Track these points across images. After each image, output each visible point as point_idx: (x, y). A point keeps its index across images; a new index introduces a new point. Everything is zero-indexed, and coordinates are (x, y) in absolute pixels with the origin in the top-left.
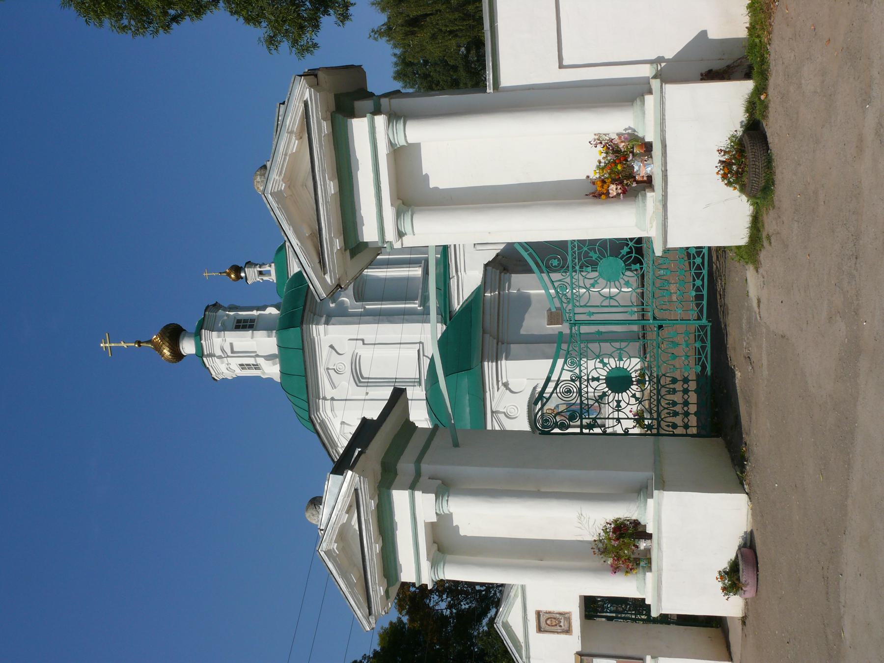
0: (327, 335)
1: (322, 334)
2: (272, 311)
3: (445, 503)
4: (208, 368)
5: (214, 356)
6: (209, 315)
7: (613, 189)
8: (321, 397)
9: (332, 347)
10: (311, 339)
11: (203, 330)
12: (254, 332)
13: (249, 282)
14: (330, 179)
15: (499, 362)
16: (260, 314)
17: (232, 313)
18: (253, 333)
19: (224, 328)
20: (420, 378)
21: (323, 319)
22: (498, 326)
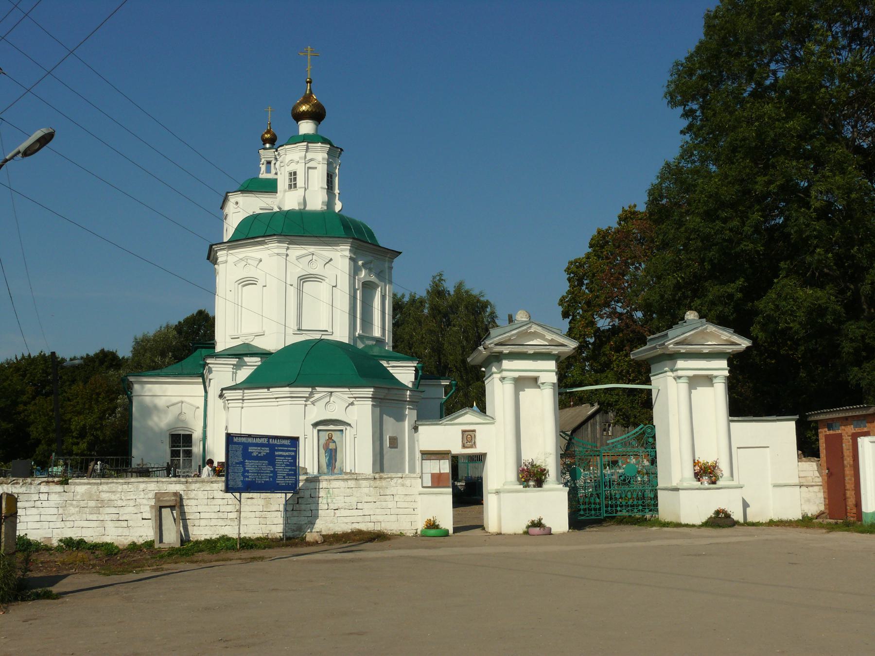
0: (341, 258)
1: (339, 254)
2: (338, 206)
3: (550, 387)
4: (296, 144)
5: (306, 152)
6: (337, 151)
7: (697, 468)
8: (289, 246)
9: (331, 260)
10: (339, 244)
11: (329, 146)
12: (326, 190)
13: (261, 151)
14: (709, 351)
15: (371, 399)
16: (336, 195)
17: (337, 171)
18: (325, 189)
19: (329, 164)
20: (301, 330)
21: (353, 256)
22: (394, 400)
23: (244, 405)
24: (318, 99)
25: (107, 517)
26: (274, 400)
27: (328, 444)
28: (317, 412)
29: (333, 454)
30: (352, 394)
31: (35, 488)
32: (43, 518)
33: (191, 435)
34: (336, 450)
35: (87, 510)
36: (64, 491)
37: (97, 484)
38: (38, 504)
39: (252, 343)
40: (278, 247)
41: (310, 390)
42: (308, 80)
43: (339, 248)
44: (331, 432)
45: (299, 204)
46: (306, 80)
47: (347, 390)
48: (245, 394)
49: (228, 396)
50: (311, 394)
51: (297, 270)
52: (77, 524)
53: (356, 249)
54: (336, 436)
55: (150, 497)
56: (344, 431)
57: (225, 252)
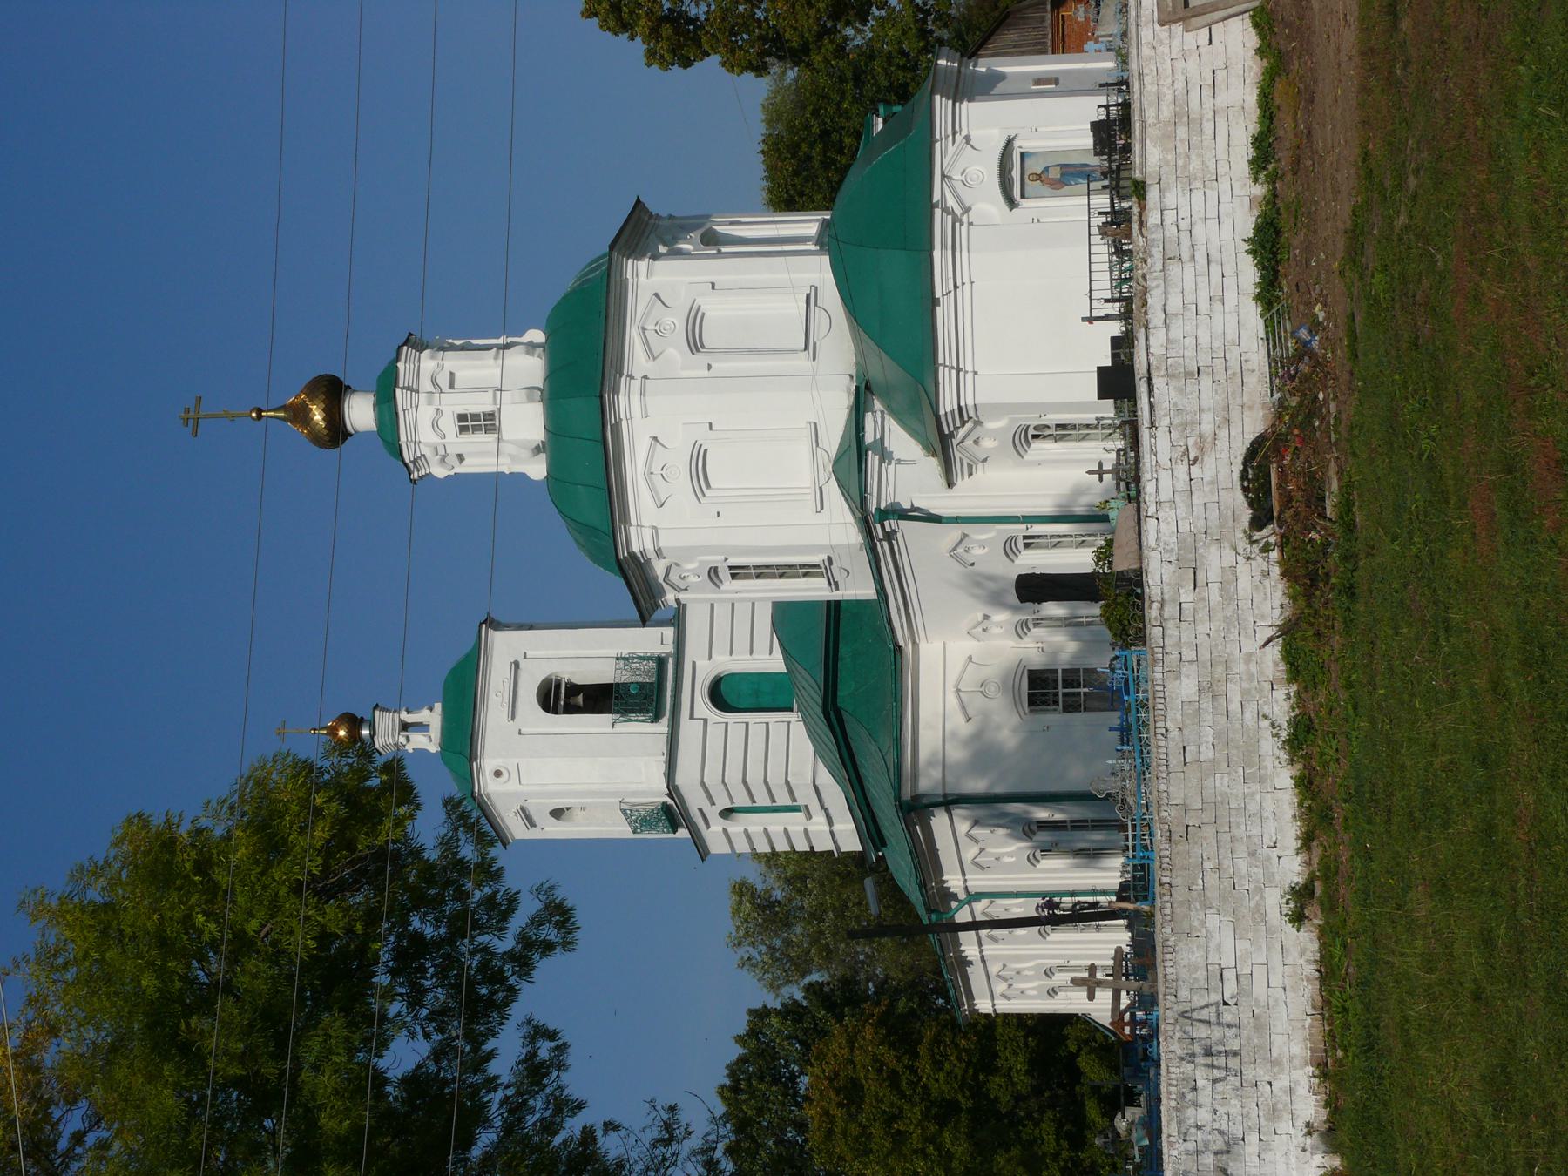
1: (642, 278)
4: (397, 414)
15: (958, 104)
23: (969, 368)
24: (298, 392)
25: (1209, 104)
26: (958, 254)
27: (1047, 432)
28: (987, 203)
29: (1072, 170)
30: (947, 137)
31: (1153, 233)
32: (1212, 213)
33: (1031, 672)
34: (1063, 166)
35: (1194, 140)
36: (1159, 183)
37: (1143, 128)
38: (1184, 225)
39: (833, 451)
40: (628, 394)
41: (938, 212)
42: (254, 415)
43: (631, 281)
44: (1026, 177)
45: (530, 400)
46: (253, 418)
47: (937, 145)
48: (947, 364)
49: (951, 402)
50: (946, 210)
51: (675, 350)
52: (1222, 155)
53: (633, 252)
54: (1034, 167)
55: (1167, 34)
56: (1022, 150)
57: (632, 530)
